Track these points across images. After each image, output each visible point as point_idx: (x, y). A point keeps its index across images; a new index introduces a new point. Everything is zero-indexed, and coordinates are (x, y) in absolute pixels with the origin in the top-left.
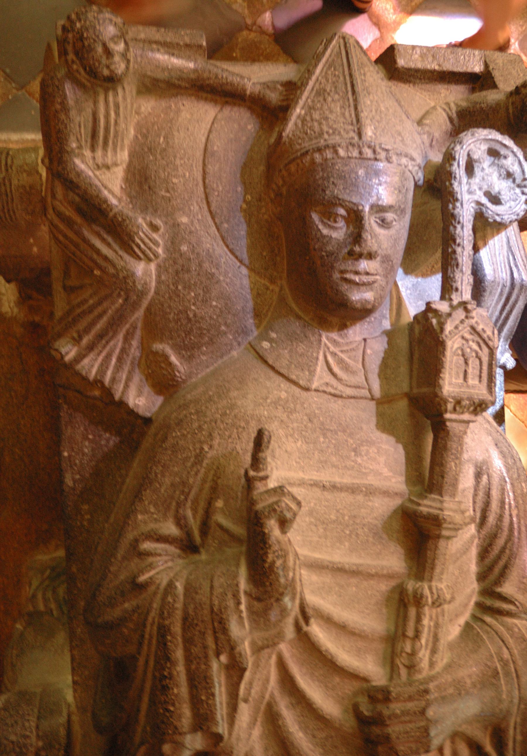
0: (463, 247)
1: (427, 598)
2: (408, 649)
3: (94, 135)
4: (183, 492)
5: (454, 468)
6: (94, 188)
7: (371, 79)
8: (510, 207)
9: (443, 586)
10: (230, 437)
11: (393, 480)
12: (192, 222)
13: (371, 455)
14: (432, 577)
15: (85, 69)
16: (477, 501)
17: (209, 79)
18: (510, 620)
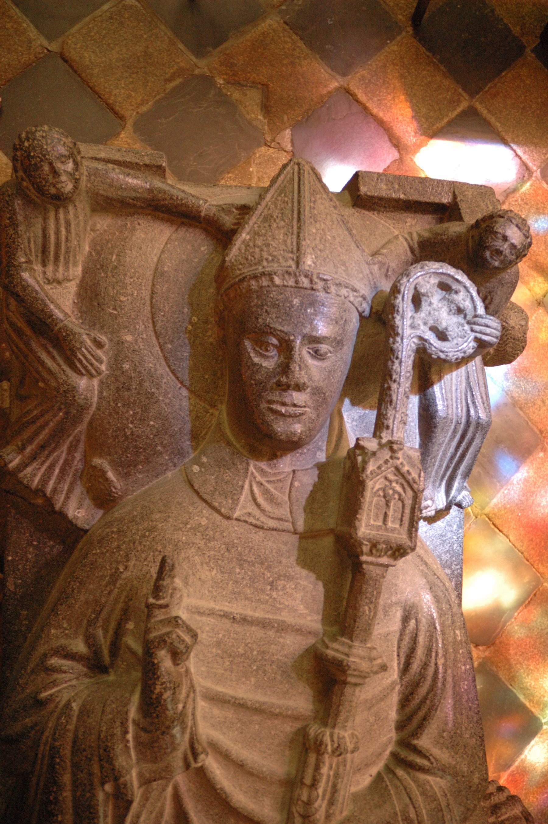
0: (399, 384)
1: (326, 746)
2: (304, 798)
3: (45, 250)
4: (94, 612)
5: (367, 612)
6: (40, 302)
7: (322, 207)
8: (457, 344)
9: (346, 735)
10: (145, 560)
11: (309, 618)
12: (136, 341)
13: (288, 590)
14: (335, 725)
15: (33, 186)
16: (402, 646)
17: (164, 199)
18: (422, 776)
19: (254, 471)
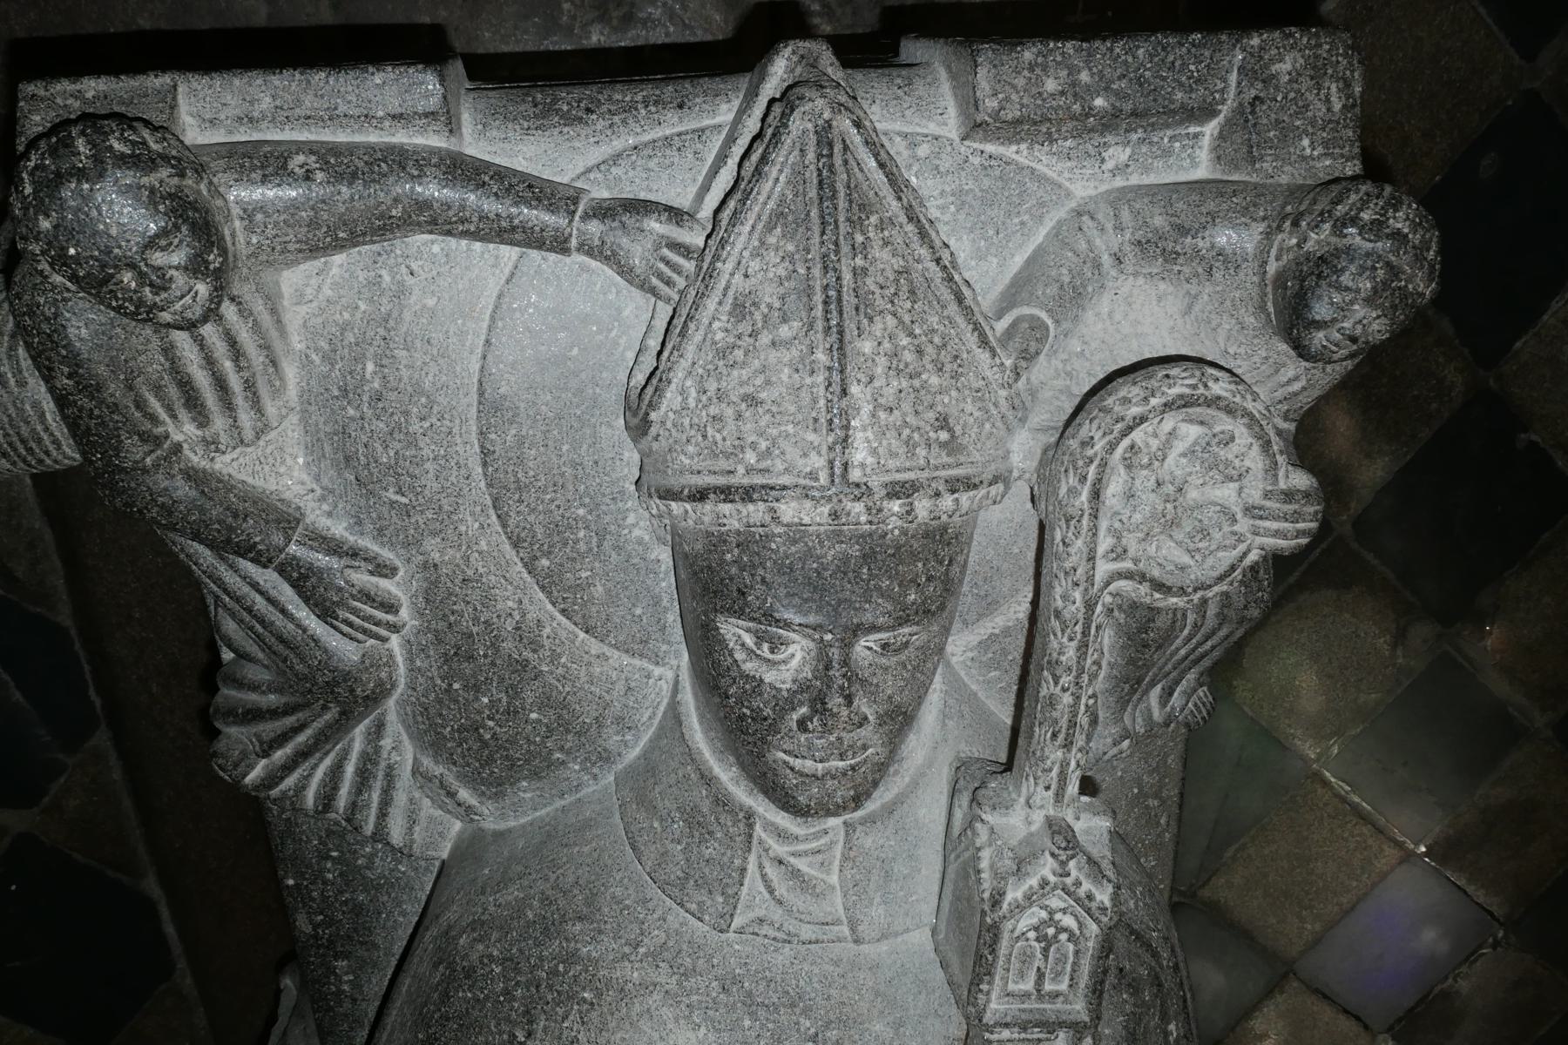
12: (467, 559)
19: (763, 835)
